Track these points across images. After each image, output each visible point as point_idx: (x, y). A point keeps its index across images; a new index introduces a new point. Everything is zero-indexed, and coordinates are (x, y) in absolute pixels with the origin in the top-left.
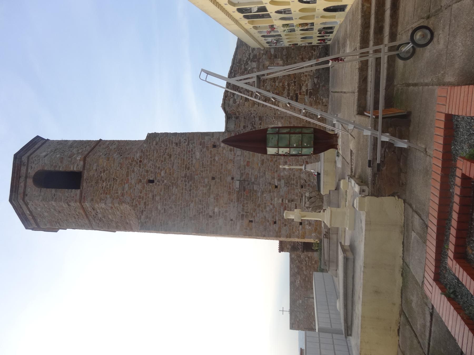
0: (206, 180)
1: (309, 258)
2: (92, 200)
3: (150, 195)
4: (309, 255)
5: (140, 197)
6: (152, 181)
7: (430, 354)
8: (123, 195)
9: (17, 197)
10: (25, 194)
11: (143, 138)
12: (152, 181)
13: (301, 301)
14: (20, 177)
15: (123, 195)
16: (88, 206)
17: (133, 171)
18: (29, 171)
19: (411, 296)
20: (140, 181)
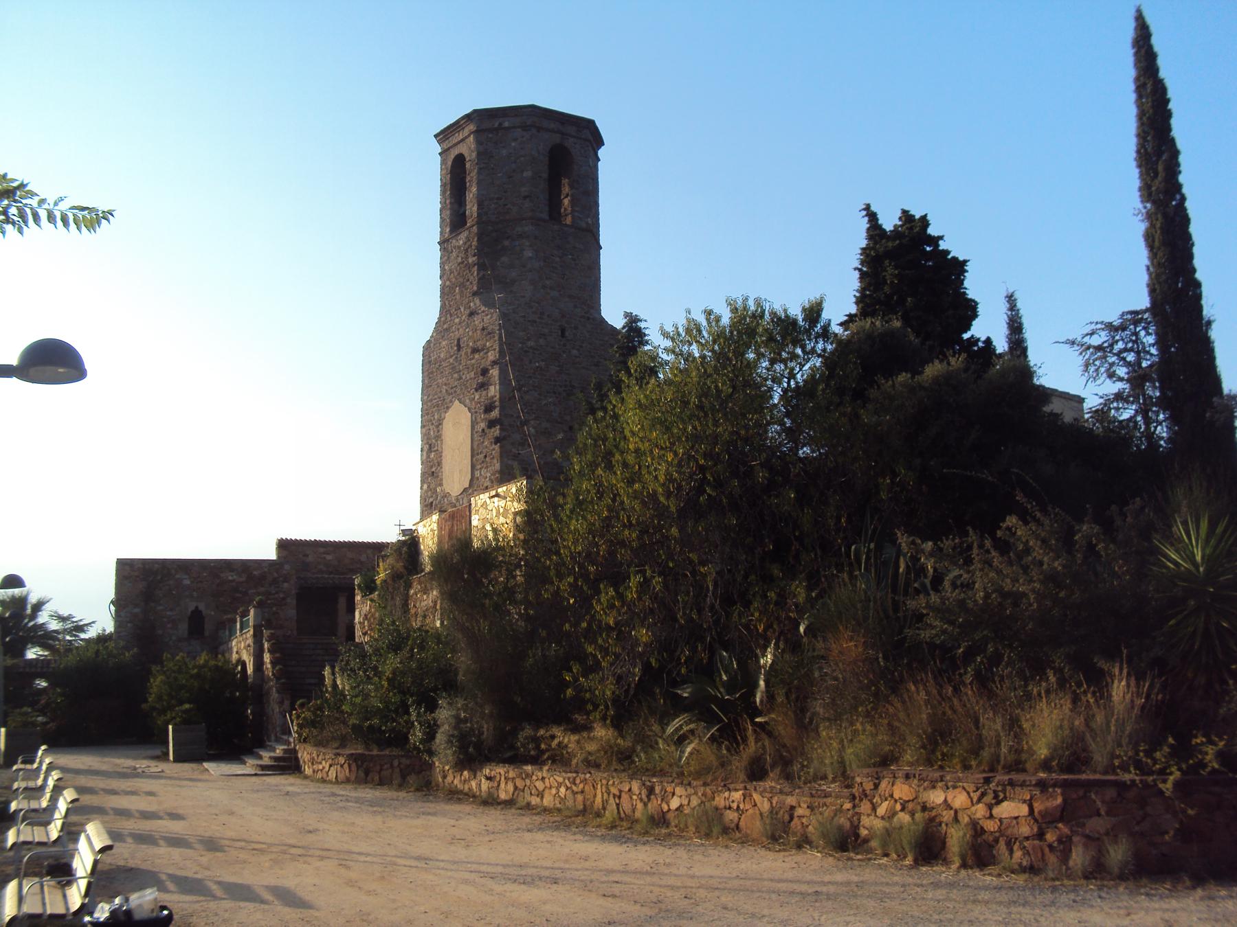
0: (568, 418)
1: (284, 599)
2: (536, 238)
3: (546, 331)
4: (289, 600)
5: (542, 313)
6: (563, 335)
7: (85, 808)
8: (544, 287)
9: (487, 123)
10: (539, 129)
11: (971, 294)
12: (563, 335)
13: (187, 582)
14: (563, 124)
15: (544, 287)
16: (526, 229)
17: (575, 307)
18: (572, 140)
19: (360, 750)
20: (563, 316)
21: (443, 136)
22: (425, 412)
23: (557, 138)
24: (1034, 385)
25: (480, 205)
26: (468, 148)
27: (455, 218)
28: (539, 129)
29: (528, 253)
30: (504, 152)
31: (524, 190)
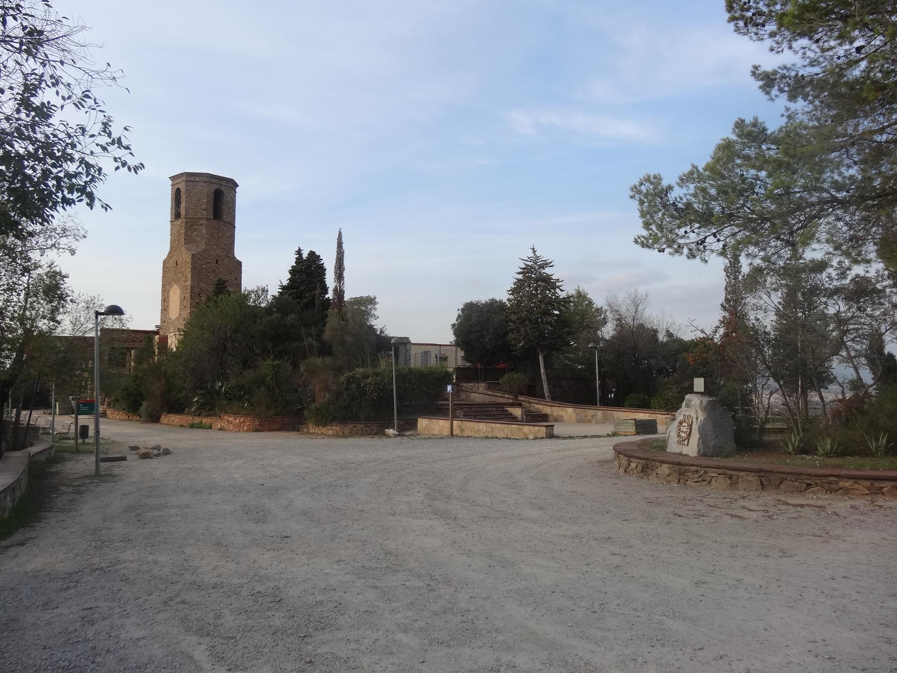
9: (191, 178)
21: (173, 178)
22: (163, 286)
23: (218, 187)
24: (269, 310)
25: (186, 211)
26: (182, 187)
27: (177, 215)
29: (204, 232)
31: (204, 207)
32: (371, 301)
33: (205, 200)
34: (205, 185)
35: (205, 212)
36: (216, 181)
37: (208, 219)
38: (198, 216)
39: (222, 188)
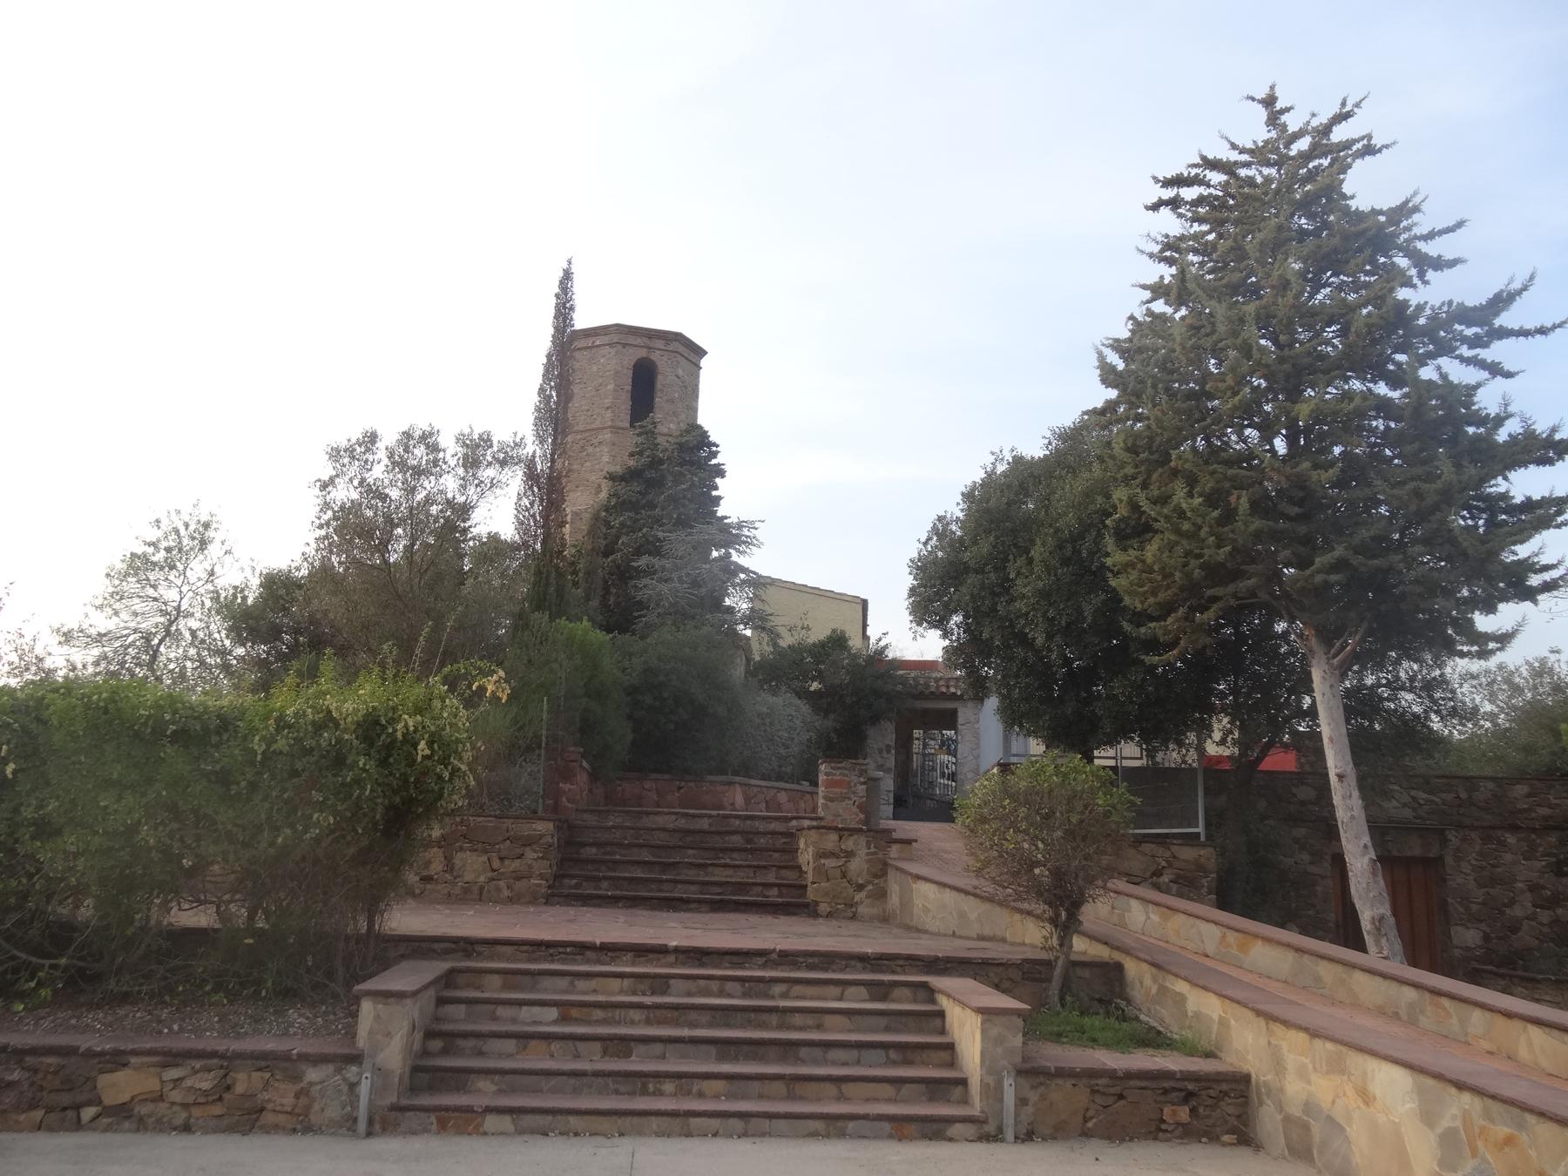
10: (624, 345)
23: (643, 353)
28: (624, 345)
30: (595, 368)
31: (608, 401)
32: (705, 353)
33: (610, 387)
34: (613, 351)
35: (609, 414)
36: (639, 341)
37: (615, 429)
38: (598, 424)
39: (655, 356)
